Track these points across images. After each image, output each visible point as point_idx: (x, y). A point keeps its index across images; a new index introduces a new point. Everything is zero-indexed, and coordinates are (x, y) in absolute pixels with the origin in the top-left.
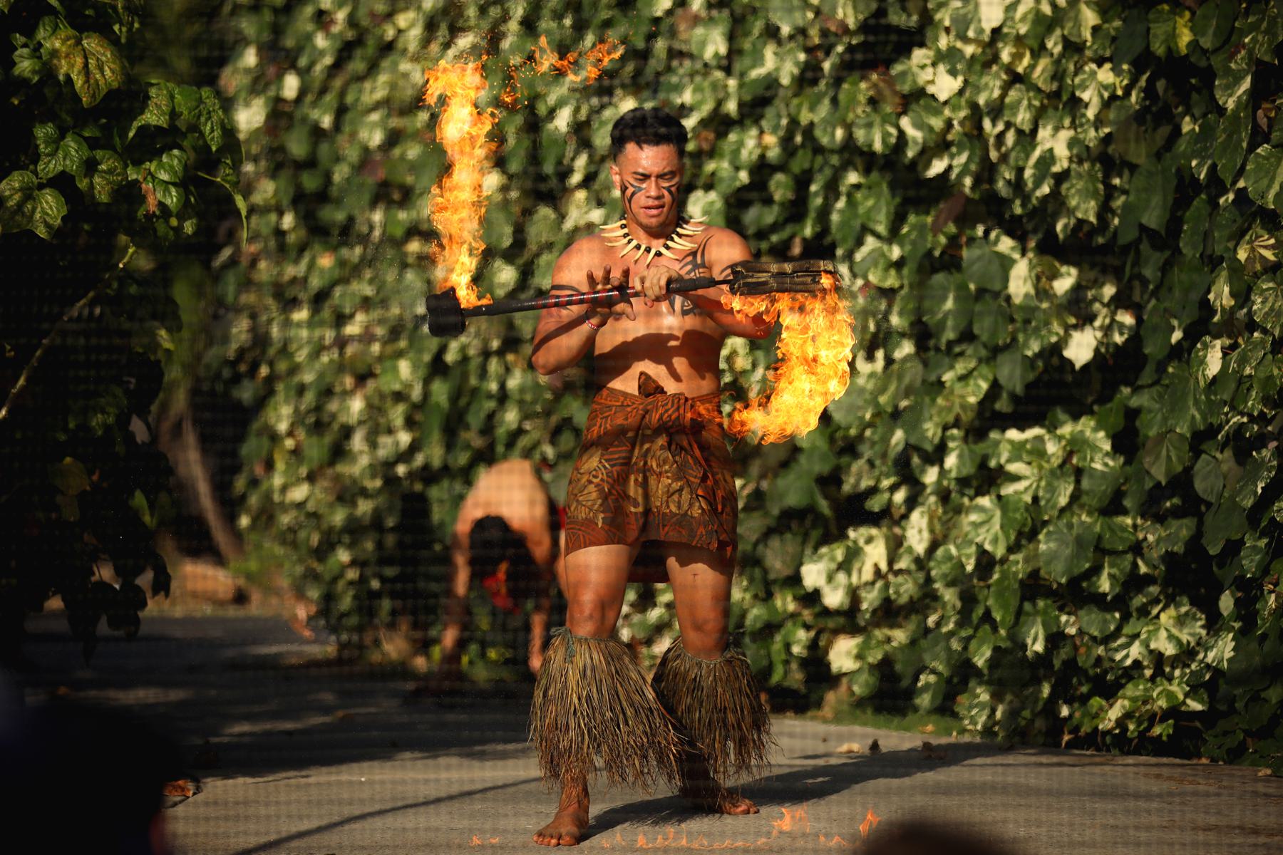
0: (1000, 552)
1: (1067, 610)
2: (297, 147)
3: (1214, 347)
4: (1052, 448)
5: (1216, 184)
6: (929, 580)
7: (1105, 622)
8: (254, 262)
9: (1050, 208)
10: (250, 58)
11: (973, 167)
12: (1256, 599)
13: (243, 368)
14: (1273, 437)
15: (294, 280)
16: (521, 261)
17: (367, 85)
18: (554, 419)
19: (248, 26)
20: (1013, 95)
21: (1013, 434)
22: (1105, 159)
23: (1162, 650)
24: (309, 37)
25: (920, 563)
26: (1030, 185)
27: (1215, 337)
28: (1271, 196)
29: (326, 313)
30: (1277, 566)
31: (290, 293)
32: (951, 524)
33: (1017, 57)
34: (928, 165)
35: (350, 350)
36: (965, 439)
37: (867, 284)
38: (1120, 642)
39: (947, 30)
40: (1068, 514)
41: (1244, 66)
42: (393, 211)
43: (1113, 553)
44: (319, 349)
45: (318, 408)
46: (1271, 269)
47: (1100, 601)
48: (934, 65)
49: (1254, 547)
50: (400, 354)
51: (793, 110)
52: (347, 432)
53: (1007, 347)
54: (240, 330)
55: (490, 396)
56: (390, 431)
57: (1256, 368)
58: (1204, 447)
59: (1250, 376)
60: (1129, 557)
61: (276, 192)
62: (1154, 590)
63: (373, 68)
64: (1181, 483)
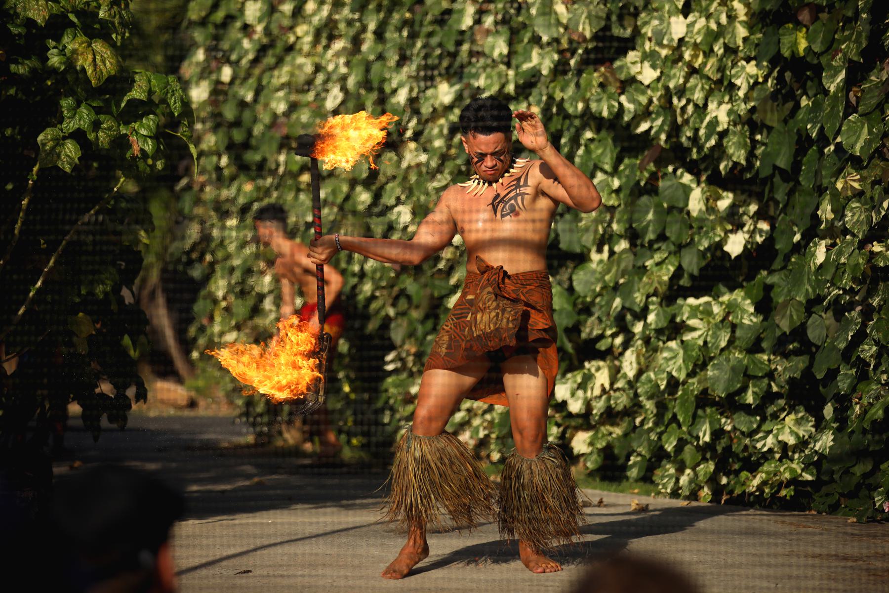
0: (682, 377)
3: (820, 245)
4: (716, 309)
5: (823, 140)
6: (636, 395)
9: (716, 155)
10: (200, 55)
14: (858, 303)
16: (374, 188)
17: (276, 73)
18: (396, 289)
19: (198, 35)
20: (692, 81)
21: (691, 301)
22: (751, 123)
24: (239, 42)
31: (226, 207)
32: (651, 359)
33: (695, 56)
38: (761, 435)
39: (650, 39)
40: (727, 352)
44: (243, 245)
45: (243, 282)
47: (747, 409)
52: (261, 297)
54: (194, 232)
57: (848, 259)
58: (814, 310)
59: (844, 264)
60: (766, 381)
61: (216, 142)
62: (782, 402)
63: (280, 62)
64: (799, 332)
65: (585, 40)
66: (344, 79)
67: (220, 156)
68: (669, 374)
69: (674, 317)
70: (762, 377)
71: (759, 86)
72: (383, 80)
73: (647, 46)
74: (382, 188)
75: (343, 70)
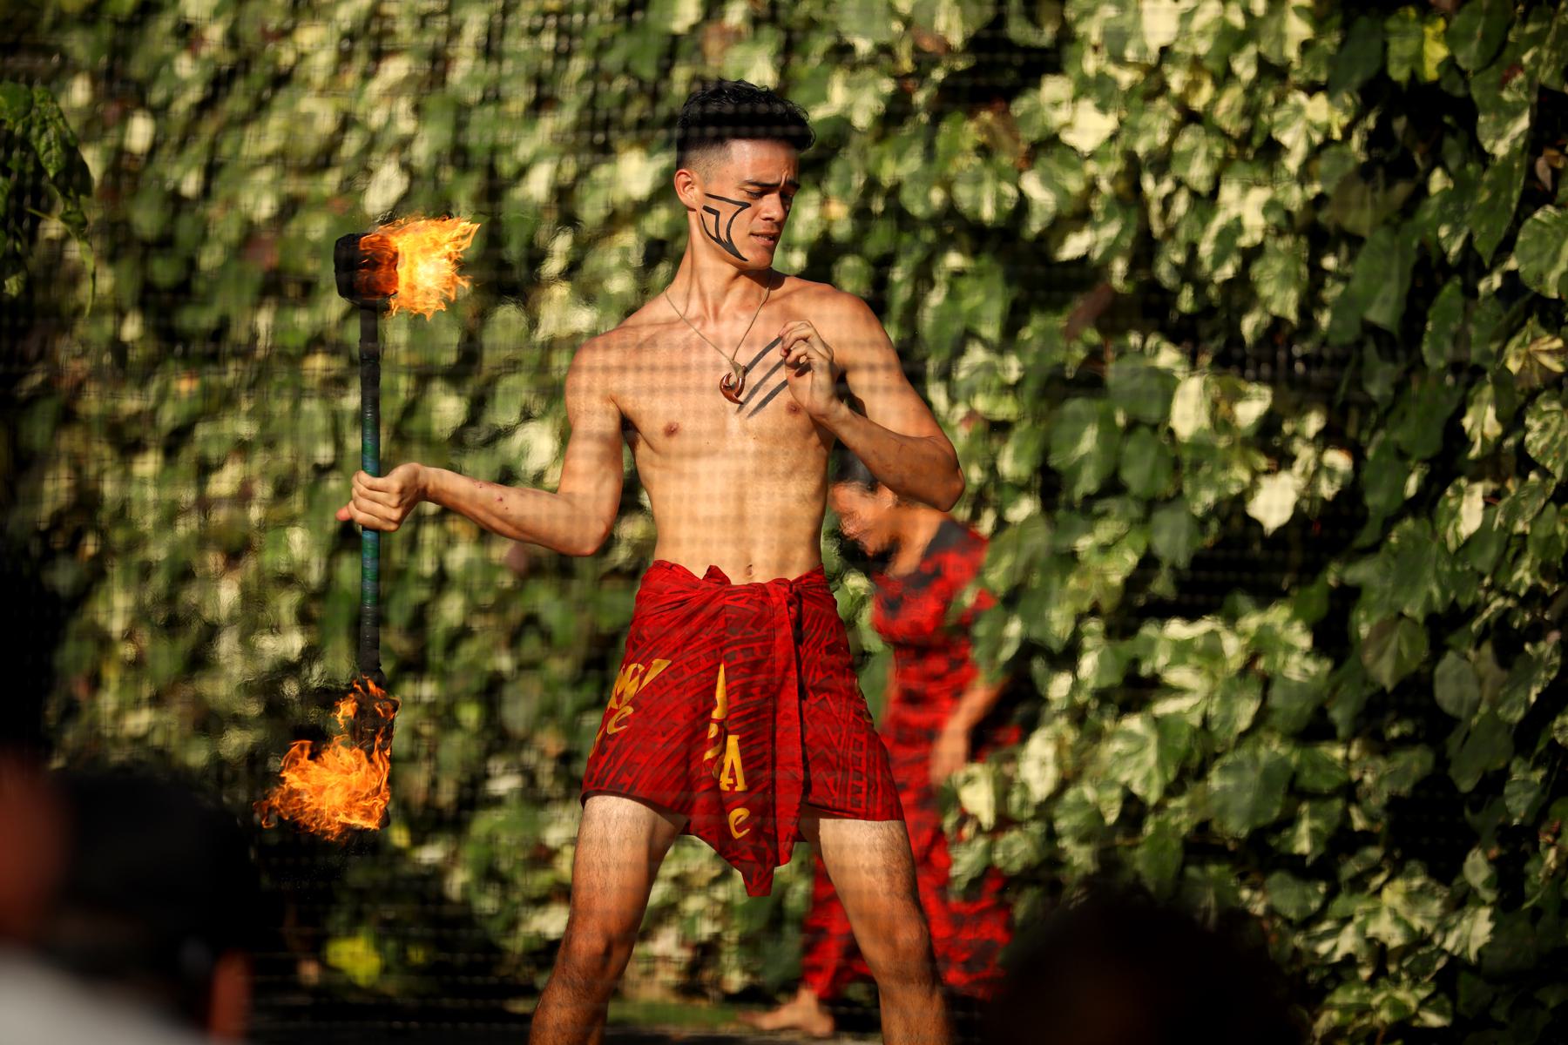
0: (1153, 797)
1: (1250, 880)
2: (146, 219)
3: (1471, 493)
4: (1232, 646)
5: (1472, 265)
6: (1051, 835)
7: (1306, 898)
8: (78, 388)
9: (1237, 299)
10: (79, 92)
11: (1127, 242)
12: (1525, 858)
13: (59, 541)
14: (1552, 626)
15: (137, 417)
16: (471, 386)
17: (251, 131)
18: (515, 614)
19: (78, 44)
20: (1186, 141)
21: (1177, 629)
22: (1313, 232)
23: (1383, 938)
24: (167, 61)
25: (1045, 811)
26: (1207, 265)
27: (1473, 479)
28: (1553, 276)
29: (187, 457)
30: (1557, 808)
31: (135, 431)
32: (1085, 756)
33: (1195, 86)
34: (1061, 242)
35: (220, 516)
36: (1109, 633)
37: (972, 415)
38: (1326, 926)
39: (1096, 49)
40: (1250, 740)
41: (1522, 96)
42: (288, 313)
43: (1314, 796)
44: (172, 514)
45: (171, 598)
46: (1554, 383)
47: (1298, 868)
48: (1075, 99)
49: (1525, 781)
50: (292, 520)
51: (871, 162)
52: (212, 631)
53: (1168, 501)
54: (56, 488)
55: (421, 579)
56: (276, 629)
57: (1532, 524)
58: (1452, 639)
59: (1523, 536)
60: (1338, 804)
61: (115, 289)
62: (1374, 853)
63: (260, 108)
64: (1414, 693)
65: (948, 49)
66: (405, 143)
67: (121, 314)
68: (1126, 788)
69: (1135, 662)
70: (1330, 796)
71: (1333, 150)
72: (494, 150)
73: (1091, 64)
74: (492, 382)
75: (405, 126)
